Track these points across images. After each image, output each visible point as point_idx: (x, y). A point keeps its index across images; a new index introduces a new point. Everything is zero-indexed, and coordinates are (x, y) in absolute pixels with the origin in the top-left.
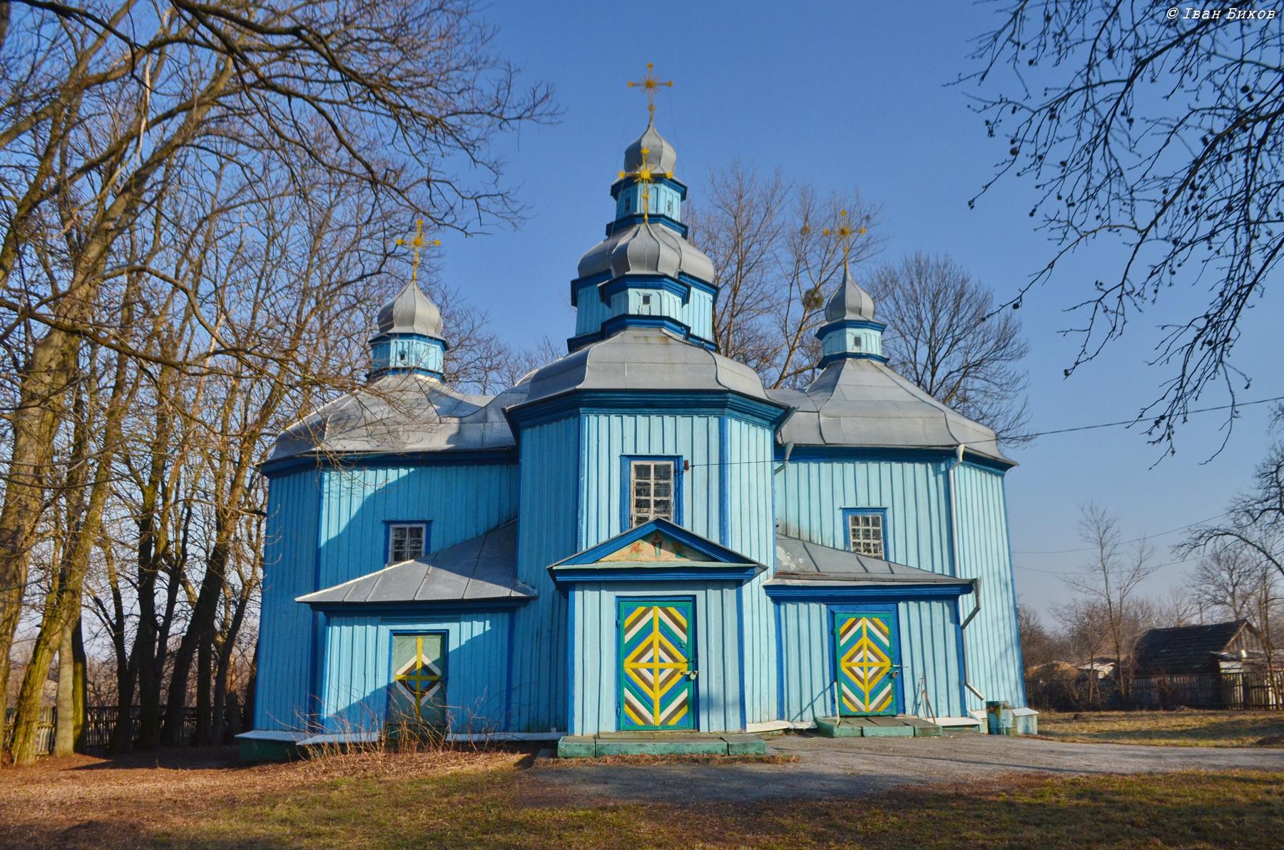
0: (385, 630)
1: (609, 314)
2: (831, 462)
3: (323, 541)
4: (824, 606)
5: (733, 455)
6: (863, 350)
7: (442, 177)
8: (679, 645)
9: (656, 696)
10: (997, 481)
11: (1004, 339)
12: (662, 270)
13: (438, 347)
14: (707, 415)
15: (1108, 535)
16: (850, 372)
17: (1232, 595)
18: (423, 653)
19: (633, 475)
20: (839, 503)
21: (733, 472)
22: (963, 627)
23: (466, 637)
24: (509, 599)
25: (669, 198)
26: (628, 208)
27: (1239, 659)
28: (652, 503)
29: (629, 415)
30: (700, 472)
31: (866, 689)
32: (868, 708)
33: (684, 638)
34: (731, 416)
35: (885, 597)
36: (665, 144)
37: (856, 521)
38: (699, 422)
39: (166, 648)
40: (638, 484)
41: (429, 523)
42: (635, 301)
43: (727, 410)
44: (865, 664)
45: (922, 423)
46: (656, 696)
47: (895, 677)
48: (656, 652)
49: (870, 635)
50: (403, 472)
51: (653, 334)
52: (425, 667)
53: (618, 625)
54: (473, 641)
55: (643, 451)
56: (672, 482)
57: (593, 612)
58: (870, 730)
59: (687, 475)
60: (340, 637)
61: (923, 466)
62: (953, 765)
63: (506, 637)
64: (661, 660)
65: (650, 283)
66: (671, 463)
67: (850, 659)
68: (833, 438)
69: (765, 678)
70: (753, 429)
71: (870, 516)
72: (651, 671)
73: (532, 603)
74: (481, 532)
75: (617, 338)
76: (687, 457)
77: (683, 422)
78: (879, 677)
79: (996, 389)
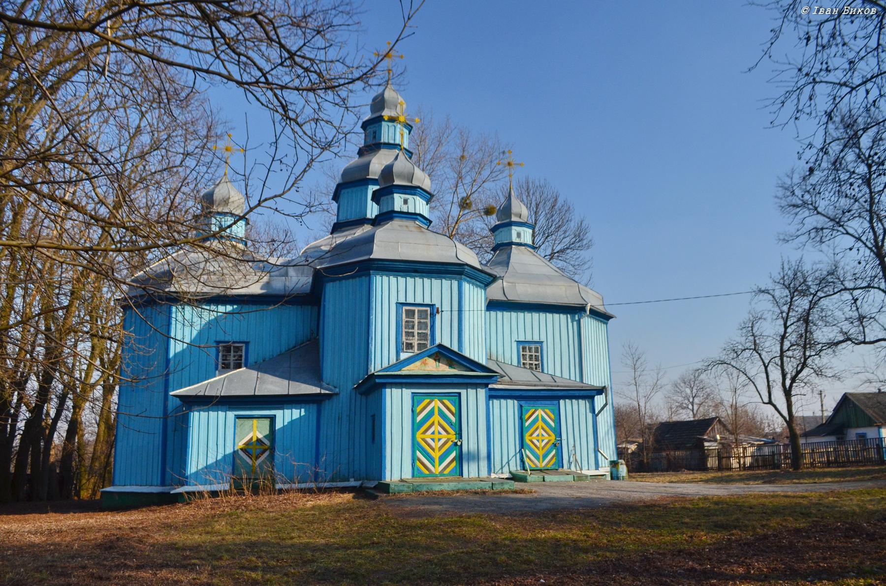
0: (231, 415)
3: (172, 354)
4: (516, 402)
5: (466, 306)
6: (522, 241)
7: (326, 118)
8: (450, 424)
9: (436, 455)
10: (604, 326)
11: (579, 236)
14: (451, 279)
15: (638, 363)
16: (516, 254)
17: (692, 404)
18: (257, 431)
20: (515, 338)
21: (466, 315)
22: (597, 415)
23: (288, 420)
24: (320, 395)
26: (375, 137)
27: (716, 440)
28: (416, 334)
29: (402, 276)
30: (446, 315)
31: (540, 453)
32: (542, 464)
33: (453, 419)
34: (465, 280)
35: (552, 396)
37: (524, 349)
38: (446, 283)
42: (398, 202)
44: (540, 438)
45: (560, 292)
46: (436, 455)
47: (557, 446)
48: (436, 428)
49: (543, 420)
50: (229, 308)
51: (410, 223)
52: (258, 440)
53: (413, 411)
54: (292, 422)
55: (410, 300)
56: (428, 321)
57: (397, 403)
58: (548, 478)
59: (438, 317)
60: (199, 419)
62: (619, 492)
63: (315, 421)
64: (439, 433)
65: (408, 191)
66: (428, 309)
67: (531, 435)
69: (494, 444)
70: (476, 289)
72: (433, 440)
73: (335, 397)
74: (283, 350)
75: (389, 226)
76: (438, 305)
77: (436, 282)
79: (571, 268)
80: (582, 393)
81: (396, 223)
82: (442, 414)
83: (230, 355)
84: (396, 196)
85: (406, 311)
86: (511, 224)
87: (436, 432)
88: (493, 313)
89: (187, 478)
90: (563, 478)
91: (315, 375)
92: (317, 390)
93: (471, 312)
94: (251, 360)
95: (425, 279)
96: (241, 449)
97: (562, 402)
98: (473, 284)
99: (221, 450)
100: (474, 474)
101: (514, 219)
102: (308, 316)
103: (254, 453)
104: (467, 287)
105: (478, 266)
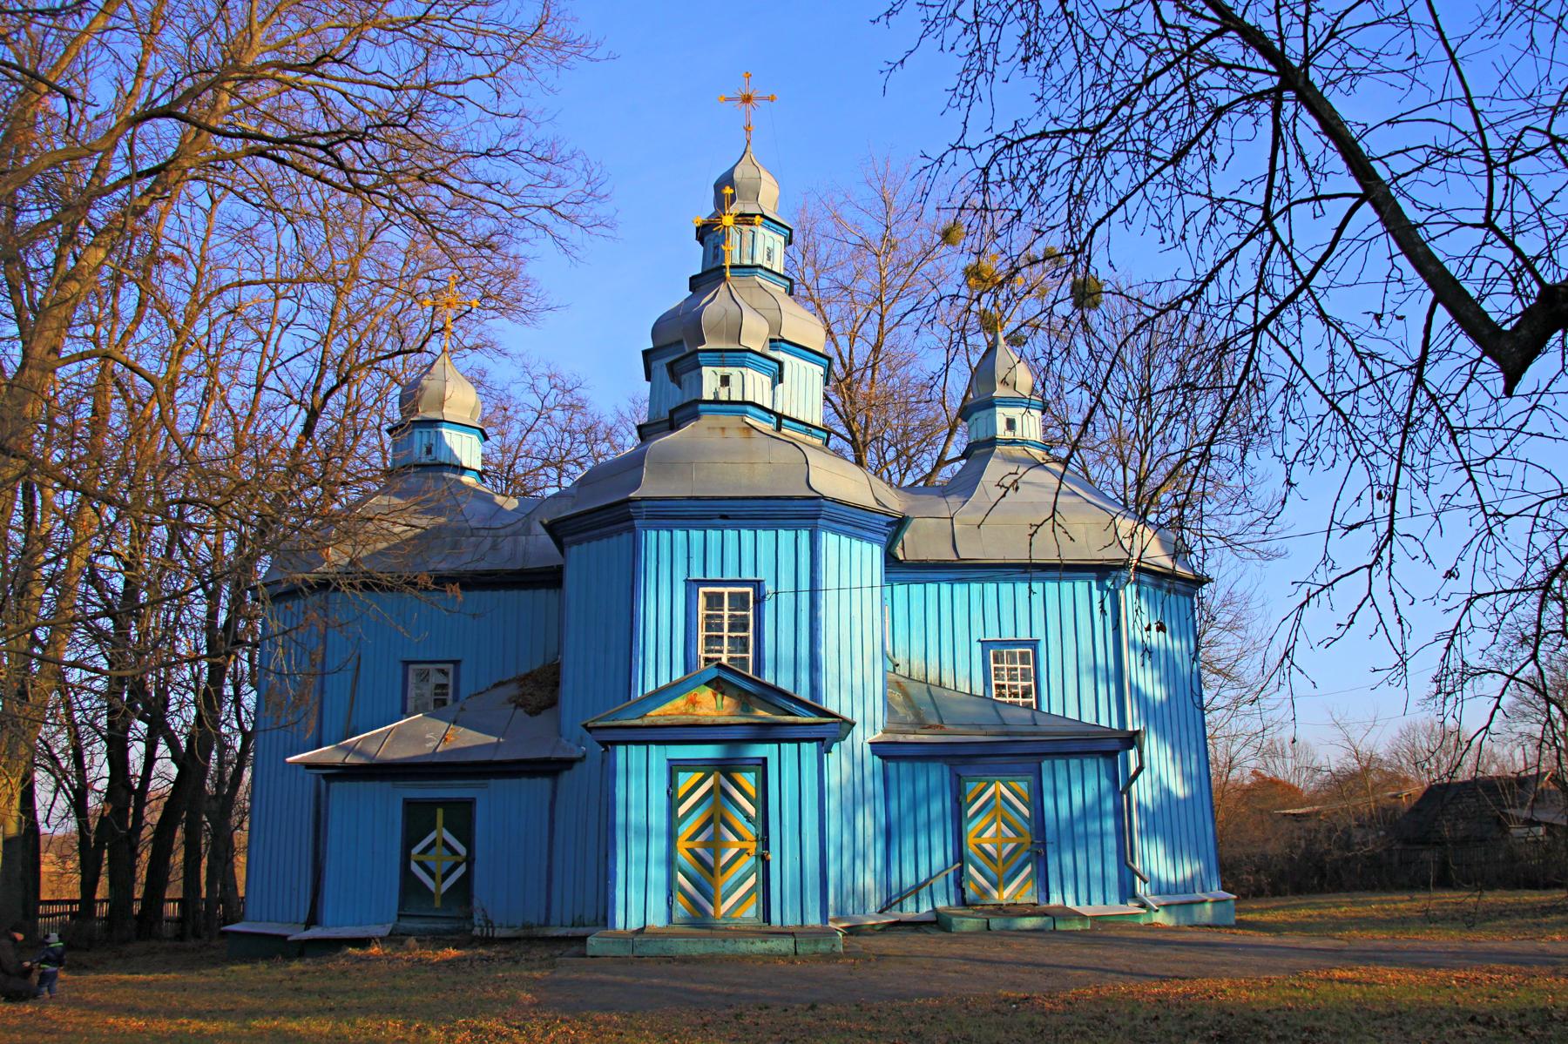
1: (677, 397)
5: (829, 579)
6: (1018, 435)
12: (746, 343)
13: (475, 438)
19: (702, 601)
20: (978, 634)
21: (828, 602)
25: (769, 243)
26: (716, 257)
36: (764, 174)
38: (786, 536)
39: (1495, 328)
40: (708, 616)
41: (456, 663)
55: (713, 574)
66: (750, 590)
67: (979, 835)
68: (969, 551)
81: (706, 420)
84: (707, 372)
85: (708, 596)
88: (900, 590)
93: (845, 594)
97: (1046, 764)
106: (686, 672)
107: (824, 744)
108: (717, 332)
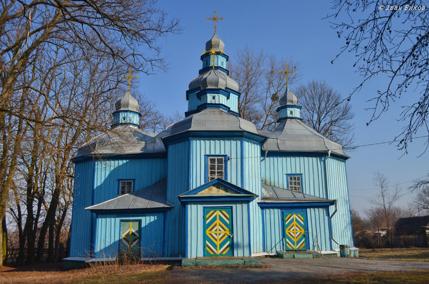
0: (118, 220)
1: (200, 103)
2: (282, 157)
3: (95, 187)
4: (279, 210)
5: (246, 154)
6: (293, 116)
7: (138, 53)
8: (226, 224)
9: (218, 243)
10: (343, 164)
11: (346, 111)
12: (219, 87)
13: (137, 115)
15: (384, 183)
18: (132, 228)
19: (209, 162)
20: (285, 172)
21: (246, 161)
23: (148, 222)
25: (222, 60)
26: (207, 64)
29: (208, 140)
30: (234, 161)
31: (295, 240)
32: (296, 247)
33: (228, 222)
34: (245, 140)
35: (302, 206)
36: (220, 41)
38: (234, 142)
41: (134, 180)
43: (243, 138)
44: (295, 231)
45: (315, 143)
46: (218, 243)
47: (306, 236)
48: (218, 227)
49: (297, 220)
50: (125, 161)
51: (216, 110)
53: (204, 217)
54: (150, 223)
55: (213, 153)
56: (223, 165)
57: (195, 212)
58: (297, 256)
59: (229, 162)
61: (316, 158)
64: (220, 230)
66: (223, 158)
67: (289, 230)
71: (296, 177)
72: (216, 234)
74: (153, 183)
77: (228, 142)
78: (300, 236)
80: (320, 204)
81: (207, 111)
82: (221, 219)
83: (124, 185)
84: (208, 95)
85: (211, 159)
86: (286, 107)
87: (218, 230)
89: (95, 254)
90: (306, 256)
91: (163, 197)
92: (162, 205)
93: (253, 158)
94: (136, 189)
95: (221, 141)
96: (124, 238)
98: (251, 142)
99: (108, 239)
100: (240, 254)
101: (288, 103)
102: (160, 165)
103: (130, 240)
104: (246, 144)
105: (256, 132)
106: (205, 183)
107: (248, 202)
108: (211, 84)
